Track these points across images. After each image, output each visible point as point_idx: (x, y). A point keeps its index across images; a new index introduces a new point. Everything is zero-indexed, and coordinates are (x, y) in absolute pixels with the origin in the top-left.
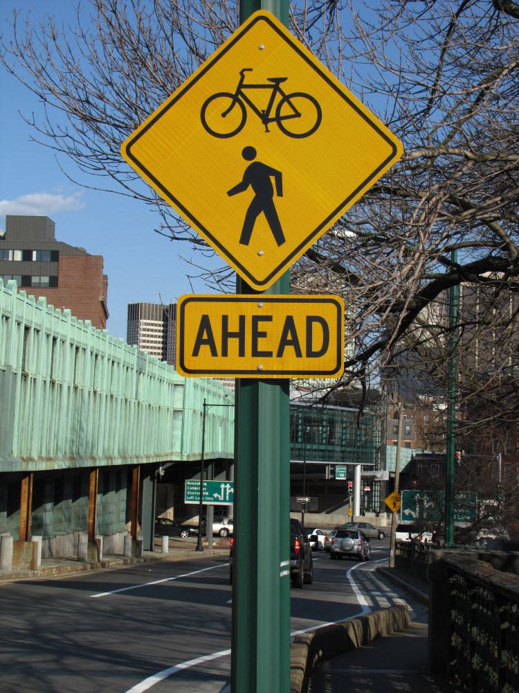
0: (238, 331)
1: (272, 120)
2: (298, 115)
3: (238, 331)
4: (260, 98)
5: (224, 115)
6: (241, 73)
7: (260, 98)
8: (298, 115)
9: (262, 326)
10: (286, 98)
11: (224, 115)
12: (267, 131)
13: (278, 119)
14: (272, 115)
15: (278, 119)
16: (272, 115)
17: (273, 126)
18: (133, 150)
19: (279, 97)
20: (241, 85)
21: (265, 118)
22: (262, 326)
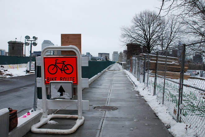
0: (88, 66)
1: (63, 70)
2: (68, 69)
3: (88, 66)
4: (60, 66)
5: (53, 69)
6: (56, 60)
7: (60, 66)
8: (68, 69)
9: (74, 78)
10: (66, 66)
11: (53, 69)
12: (62, 73)
13: (64, 70)
14: (63, 69)
15: (64, 70)
16: (63, 69)
17: (63, 72)
18: (71, 84)
19: (64, 65)
20: (56, 63)
21: (61, 70)
22: (74, 78)
